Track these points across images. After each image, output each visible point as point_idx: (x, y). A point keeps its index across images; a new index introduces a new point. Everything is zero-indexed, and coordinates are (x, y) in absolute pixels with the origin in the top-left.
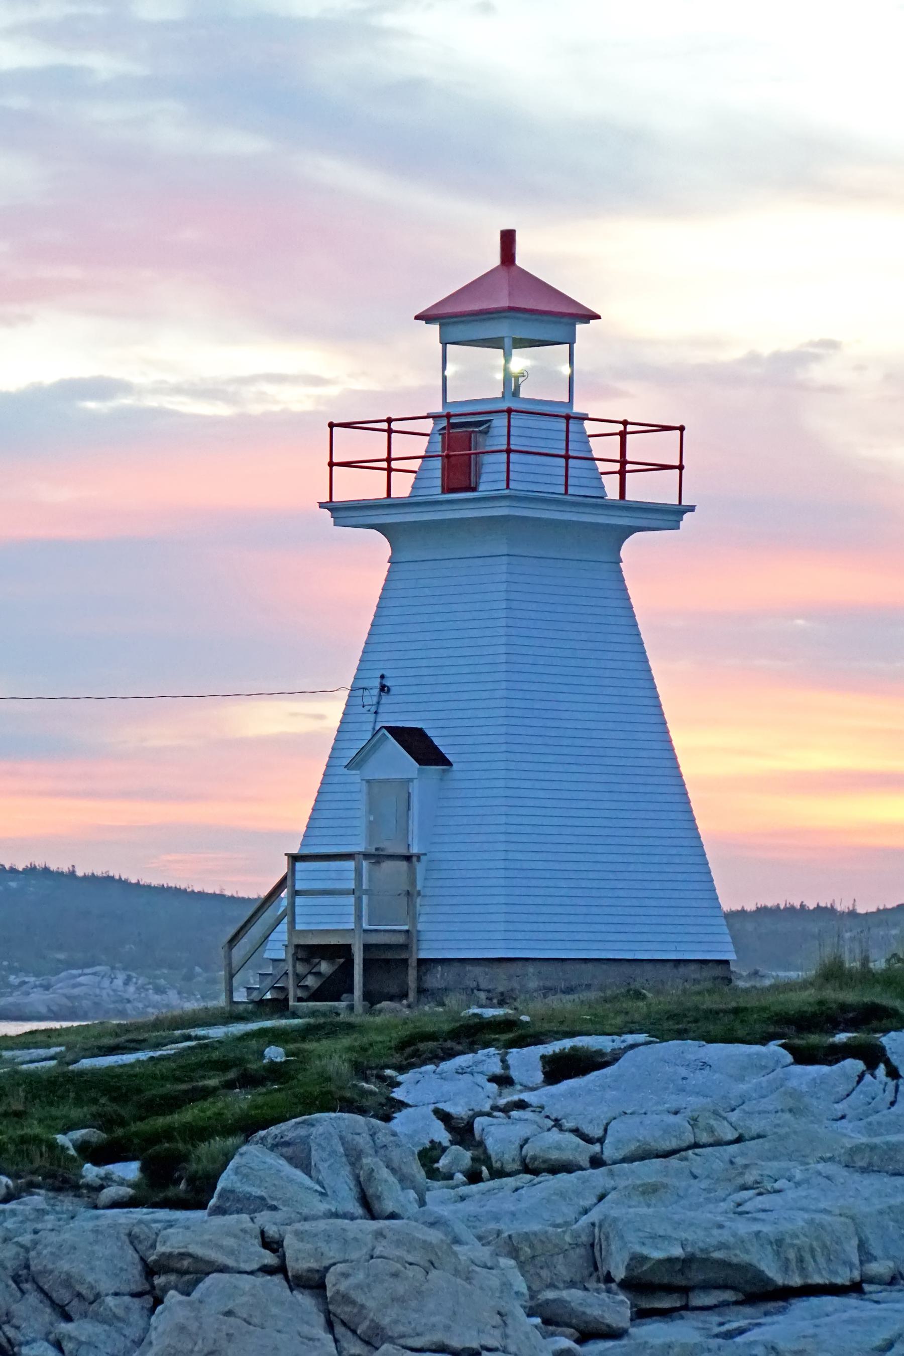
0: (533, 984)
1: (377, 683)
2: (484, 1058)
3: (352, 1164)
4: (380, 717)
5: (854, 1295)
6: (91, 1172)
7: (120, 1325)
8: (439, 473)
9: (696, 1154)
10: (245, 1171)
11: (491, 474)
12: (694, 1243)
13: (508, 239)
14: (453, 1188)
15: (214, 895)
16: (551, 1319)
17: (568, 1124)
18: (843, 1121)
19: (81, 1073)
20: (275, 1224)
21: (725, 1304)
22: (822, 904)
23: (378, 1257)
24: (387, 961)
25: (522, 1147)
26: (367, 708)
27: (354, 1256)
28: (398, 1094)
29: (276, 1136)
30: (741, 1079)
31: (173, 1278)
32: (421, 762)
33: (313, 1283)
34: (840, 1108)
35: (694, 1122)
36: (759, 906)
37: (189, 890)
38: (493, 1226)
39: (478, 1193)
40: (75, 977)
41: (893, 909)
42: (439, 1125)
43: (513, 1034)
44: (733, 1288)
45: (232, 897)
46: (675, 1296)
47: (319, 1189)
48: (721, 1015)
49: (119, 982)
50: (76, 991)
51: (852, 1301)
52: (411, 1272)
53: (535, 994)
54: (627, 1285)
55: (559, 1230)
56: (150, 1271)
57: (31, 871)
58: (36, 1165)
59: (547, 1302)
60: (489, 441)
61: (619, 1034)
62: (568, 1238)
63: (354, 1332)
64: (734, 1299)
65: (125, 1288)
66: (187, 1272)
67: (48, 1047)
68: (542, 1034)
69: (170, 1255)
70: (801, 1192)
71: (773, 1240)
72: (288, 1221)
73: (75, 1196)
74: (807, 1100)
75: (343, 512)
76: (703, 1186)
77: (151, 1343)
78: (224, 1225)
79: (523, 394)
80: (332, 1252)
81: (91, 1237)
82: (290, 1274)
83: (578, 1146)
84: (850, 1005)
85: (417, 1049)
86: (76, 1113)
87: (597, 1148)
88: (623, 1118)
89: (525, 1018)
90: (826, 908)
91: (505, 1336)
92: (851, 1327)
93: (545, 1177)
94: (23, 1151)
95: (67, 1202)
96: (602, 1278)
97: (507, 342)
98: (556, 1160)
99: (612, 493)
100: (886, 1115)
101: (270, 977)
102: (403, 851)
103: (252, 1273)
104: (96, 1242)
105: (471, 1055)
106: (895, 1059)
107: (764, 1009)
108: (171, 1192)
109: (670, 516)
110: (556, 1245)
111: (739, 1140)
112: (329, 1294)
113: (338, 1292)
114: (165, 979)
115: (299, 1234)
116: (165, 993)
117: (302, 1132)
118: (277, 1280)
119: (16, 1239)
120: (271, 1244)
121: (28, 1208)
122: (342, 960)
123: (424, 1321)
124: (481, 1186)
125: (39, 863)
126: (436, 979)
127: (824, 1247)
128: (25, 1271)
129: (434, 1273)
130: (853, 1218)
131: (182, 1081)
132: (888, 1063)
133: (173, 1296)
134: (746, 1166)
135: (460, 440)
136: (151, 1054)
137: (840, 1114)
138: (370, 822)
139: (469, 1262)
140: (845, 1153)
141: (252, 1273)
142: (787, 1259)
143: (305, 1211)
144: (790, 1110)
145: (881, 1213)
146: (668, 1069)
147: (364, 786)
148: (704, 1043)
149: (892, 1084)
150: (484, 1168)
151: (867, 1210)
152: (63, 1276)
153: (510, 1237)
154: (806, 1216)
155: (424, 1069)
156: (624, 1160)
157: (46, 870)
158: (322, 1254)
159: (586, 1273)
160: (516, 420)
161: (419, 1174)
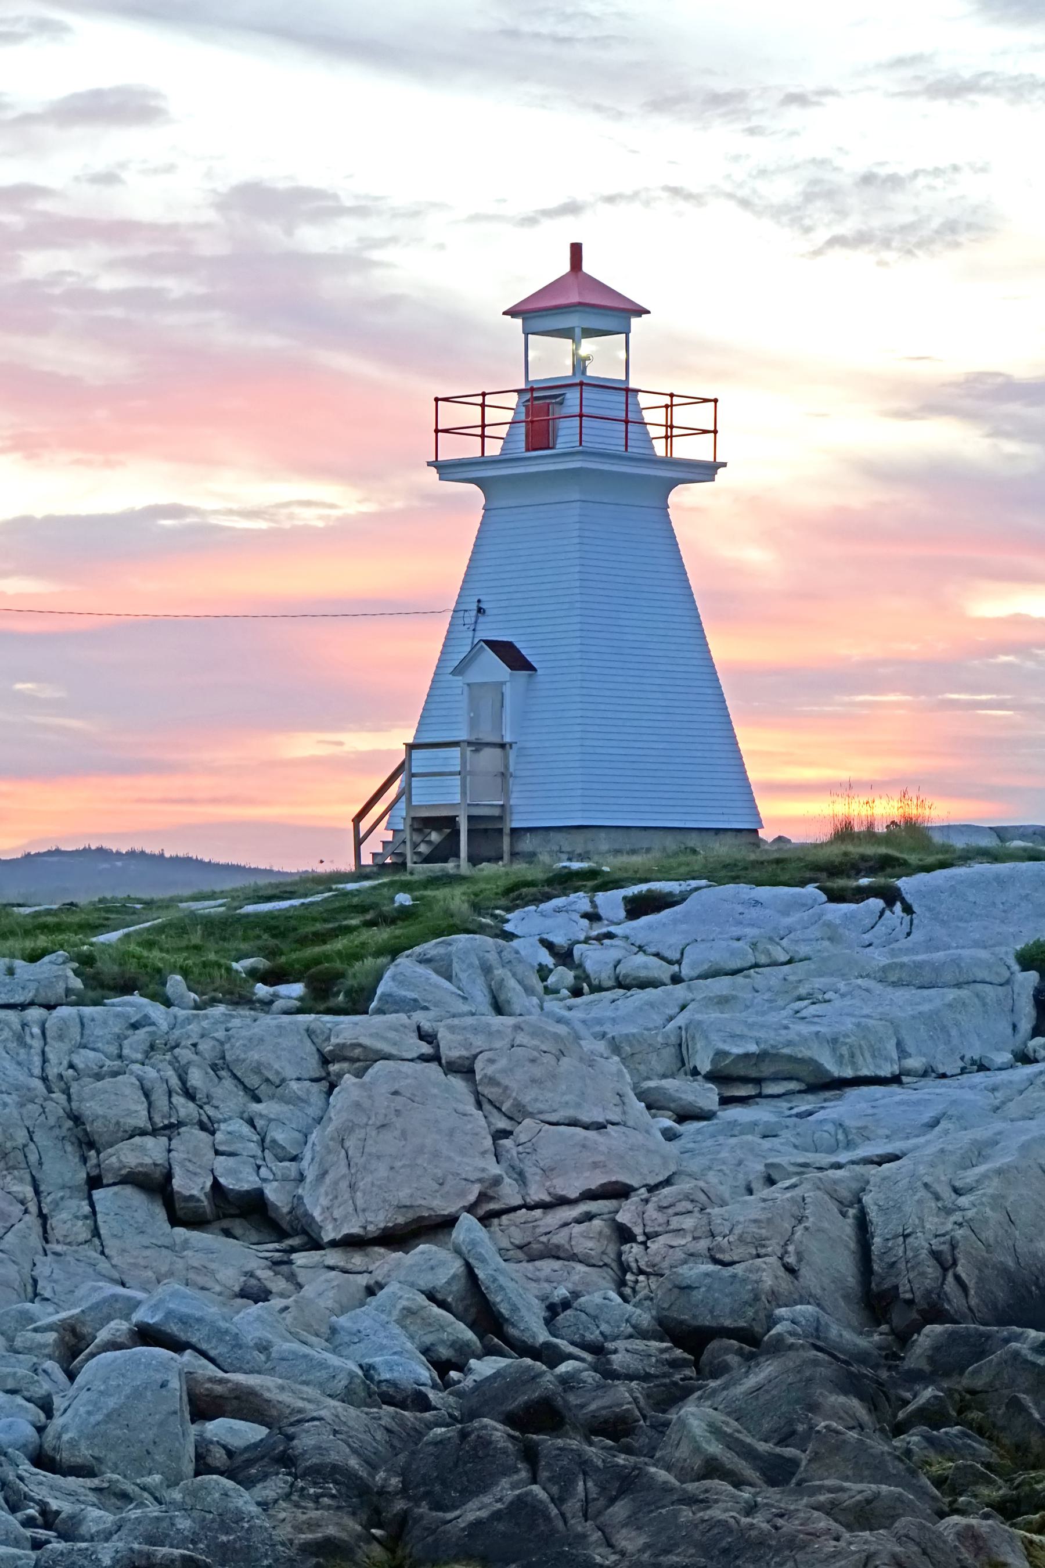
0: (604, 847)
1: (474, 606)
6: (262, 990)
8: (523, 437)
11: (566, 435)
12: (766, 1042)
13: (576, 250)
14: (561, 1000)
15: (265, 870)
17: (653, 950)
19: (247, 915)
24: (486, 830)
25: (615, 967)
27: (498, 1044)
31: (345, 1065)
32: (512, 667)
35: (754, 946)
44: (798, 1079)
51: (894, 1088)
52: (548, 1059)
54: (710, 1077)
56: (325, 1060)
57: (132, 854)
61: (685, 880)
62: (660, 1039)
63: (499, 1109)
66: (358, 1060)
68: (622, 880)
69: (343, 1046)
70: (847, 1001)
75: (446, 469)
77: (330, 1119)
79: (588, 373)
80: (479, 1042)
85: (518, 894)
86: (244, 946)
87: (676, 968)
89: (606, 869)
91: (624, 1113)
92: (903, 1108)
95: (245, 1012)
100: (904, 943)
102: (497, 740)
103: (412, 1060)
104: (280, 1035)
106: (909, 898)
107: (800, 859)
108: (332, 1003)
109: (707, 471)
111: (790, 962)
112: (478, 1078)
113: (485, 1075)
115: (452, 1029)
118: (434, 1066)
120: (424, 1036)
125: (138, 848)
126: (527, 844)
129: (565, 1061)
132: (903, 902)
133: (348, 1079)
135: (541, 411)
136: (302, 900)
141: (412, 1060)
142: (842, 1056)
143: (453, 1010)
144: (829, 939)
145: (913, 1017)
147: (466, 687)
153: (613, 1038)
154: (853, 1020)
156: (699, 977)
157: (143, 853)
159: (675, 1069)
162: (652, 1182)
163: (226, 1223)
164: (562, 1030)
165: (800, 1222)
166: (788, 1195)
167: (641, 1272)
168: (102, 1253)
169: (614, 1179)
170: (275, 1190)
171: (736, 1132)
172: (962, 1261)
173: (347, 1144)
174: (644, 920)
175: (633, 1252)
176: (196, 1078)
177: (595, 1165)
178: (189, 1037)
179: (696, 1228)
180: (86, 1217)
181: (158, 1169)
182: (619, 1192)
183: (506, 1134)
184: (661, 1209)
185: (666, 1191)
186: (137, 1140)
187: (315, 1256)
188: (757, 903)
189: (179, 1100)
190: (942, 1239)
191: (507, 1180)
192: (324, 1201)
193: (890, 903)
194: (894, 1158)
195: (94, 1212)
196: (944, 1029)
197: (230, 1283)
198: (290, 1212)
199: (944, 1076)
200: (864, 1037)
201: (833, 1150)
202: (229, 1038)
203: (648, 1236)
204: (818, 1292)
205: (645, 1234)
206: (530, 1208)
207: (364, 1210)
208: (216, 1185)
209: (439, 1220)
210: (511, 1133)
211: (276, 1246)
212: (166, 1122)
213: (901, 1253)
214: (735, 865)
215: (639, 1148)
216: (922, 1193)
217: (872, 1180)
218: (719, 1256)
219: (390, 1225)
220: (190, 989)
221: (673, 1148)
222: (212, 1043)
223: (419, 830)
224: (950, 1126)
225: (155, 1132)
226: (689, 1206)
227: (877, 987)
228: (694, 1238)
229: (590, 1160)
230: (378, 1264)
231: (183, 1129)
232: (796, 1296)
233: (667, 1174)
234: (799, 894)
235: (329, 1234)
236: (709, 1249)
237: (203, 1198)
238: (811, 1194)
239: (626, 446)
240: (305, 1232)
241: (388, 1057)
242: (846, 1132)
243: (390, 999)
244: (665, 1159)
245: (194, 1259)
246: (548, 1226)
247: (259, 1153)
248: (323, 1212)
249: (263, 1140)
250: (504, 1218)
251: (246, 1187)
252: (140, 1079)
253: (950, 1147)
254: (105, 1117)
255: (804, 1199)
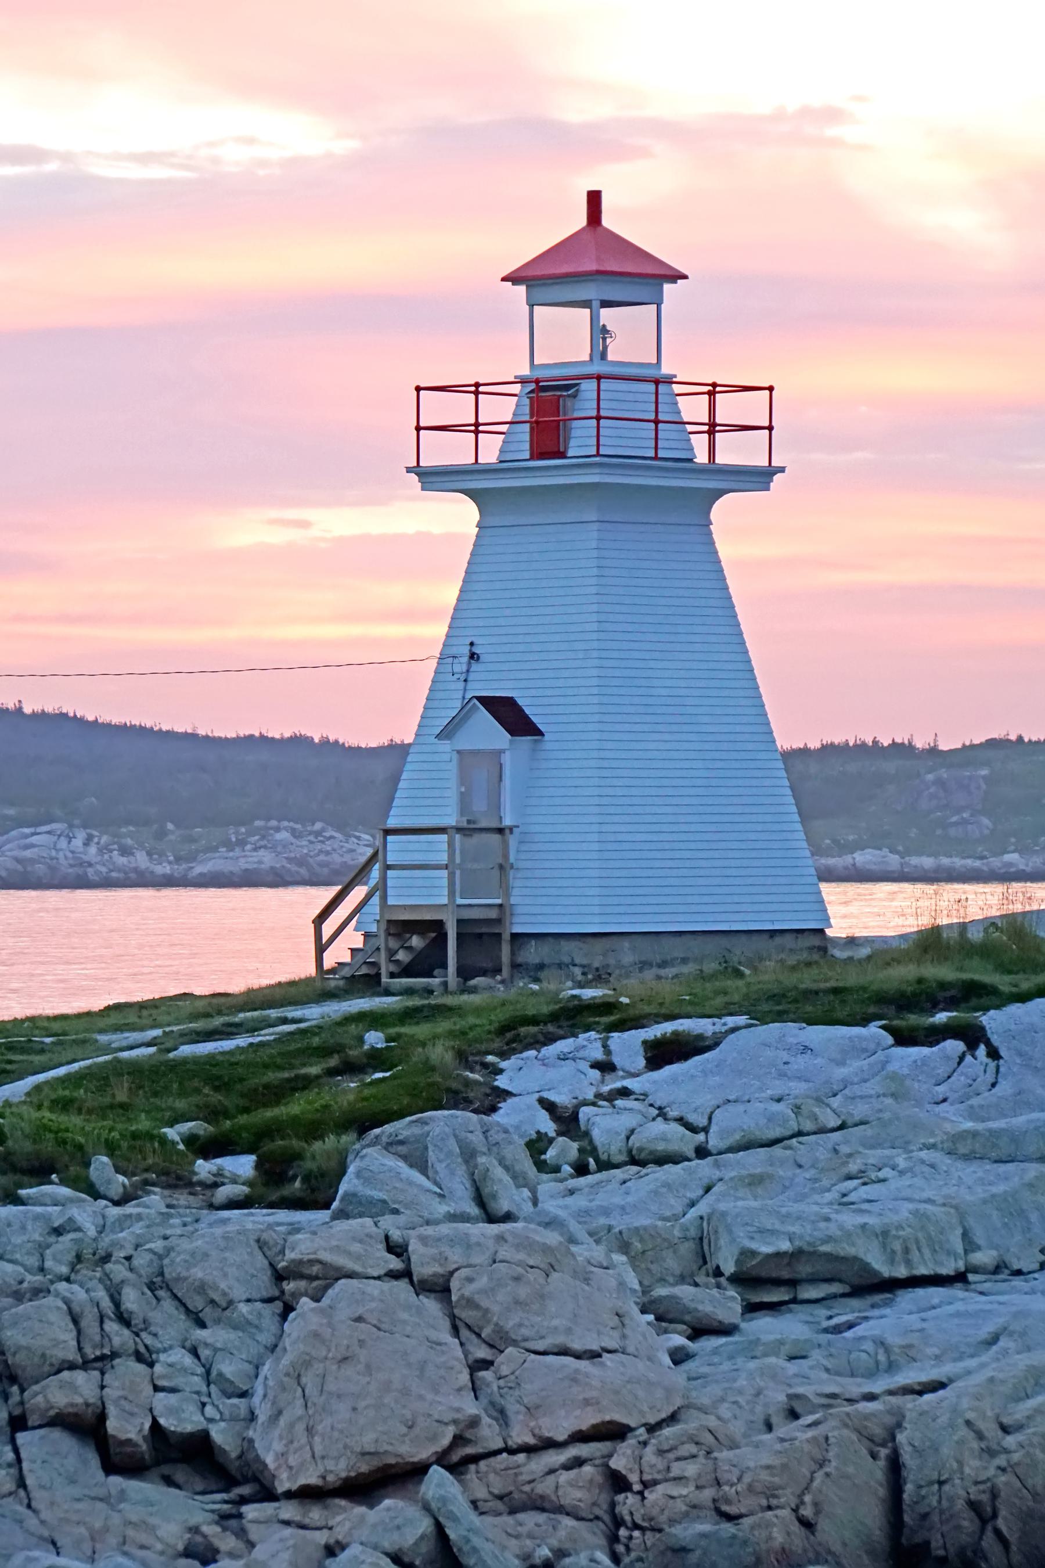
0: (628, 958)
1: (466, 650)
2: (585, 1043)
3: (466, 1162)
4: (470, 685)
5: (959, 1285)
6: (204, 1168)
7: (254, 1330)
8: (527, 437)
9: (800, 1143)
10: (367, 1174)
11: (580, 440)
12: (801, 1237)
13: (594, 199)
14: (561, 1181)
15: (186, 735)
16: (664, 1316)
17: (673, 1113)
18: (945, 1104)
19: (184, 1061)
20: (399, 1228)
21: (835, 1296)
22: (898, 740)
23: (500, 1261)
24: (480, 936)
26: (456, 676)
27: (476, 1260)
28: (501, 1082)
29: (391, 1135)
30: (841, 1063)
31: (302, 1284)
32: (512, 733)
33: (438, 1288)
34: (941, 1090)
35: (797, 1109)
36: (825, 743)
37: (155, 729)
38: (602, 1221)
39: (586, 1186)
40: (27, 836)
41: (981, 744)
42: (544, 1115)
43: (612, 1017)
44: (840, 1281)
45: (207, 736)
46: (783, 1289)
47: (438, 1191)
48: (821, 994)
49: (78, 843)
50: (28, 853)
51: (956, 1292)
52: (532, 1275)
53: (631, 969)
54: (740, 1280)
55: (669, 1224)
56: (279, 1277)
58: (150, 1161)
59: (660, 1299)
60: (578, 404)
61: (719, 1017)
62: (677, 1233)
63: (479, 1335)
64: (841, 1291)
65: (256, 1295)
66: (316, 1278)
67: (142, 1029)
68: (647, 1016)
69: (301, 1262)
70: (906, 1181)
71: (879, 1232)
72: (410, 1225)
73: (191, 1194)
74: (908, 1082)
75: (433, 478)
76: (808, 1177)
77: (285, 1350)
78: (350, 1230)
80: (455, 1257)
81: (222, 1244)
82: (415, 1279)
83: (684, 1135)
84: (950, 983)
85: (519, 1033)
86: (181, 1104)
87: (701, 1137)
88: (726, 1106)
89: (625, 1000)
90: (903, 744)
91: (624, 1337)
93: (651, 1168)
94: (135, 1148)
96: (711, 1271)
97: (596, 304)
98: (663, 1151)
99: (701, 457)
100: (987, 1097)
101: (361, 953)
102: (494, 825)
103: (379, 1278)
105: (571, 1040)
106: (995, 1040)
107: (864, 989)
108: (286, 1191)
109: (760, 477)
110: (665, 1240)
111: (842, 1127)
112: (454, 1298)
113: (462, 1297)
114: (132, 839)
115: (424, 1240)
116: (132, 854)
117: (416, 1130)
118: (403, 1284)
119: (147, 1246)
120: (396, 1249)
121: (153, 1211)
122: (433, 935)
123: (545, 1324)
124: (589, 1179)
126: (531, 954)
127: (929, 1238)
128: (159, 1279)
129: (555, 1275)
130: (956, 1208)
131: (280, 1068)
132: (988, 1044)
133: (305, 1303)
134: (850, 1155)
135: (549, 407)
137: (941, 1097)
138: (462, 793)
139: (586, 1264)
140: (947, 1140)
141: (379, 1278)
142: (893, 1252)
144: (893, 1095)
145: (985, 1202)
146: (769, 1053)
148: (804, 1025)
149: (992, 1065)
150: (591, 1160)
151: (972, 1198)
152: (196, 1283)
153: (620, 1232)
154: (911, 1206)
155: (525, 1054)
158: (446, 1259)
160: (605, 384)
161: (527, 1165)
162: (652, 1420)
163: (166, 1469)
164: (552, 1238)
165: (821, 1466)
166: (810, 1434)
167: (636, 1526)
168: (29, 1506)
169: (607, 1418)
170: (223, 1431)
171: (758, 1354)
172: (1003, 1512)
173: (304, 1380)
174: (668, 1070)
175: (627, 1503)
176: (132, 1299)
177: (587, 1402)
178: (122, 1247)
179: (699, 1475)
180: (10, 1465)
181: (90, 1410)
182: (613, 1433)
183: (486, 1364)
184: (661, 1452)
185: (667, 1431)
186: (66, 1374)
187: (268, 1509)
188: (806, 1049)
189: (112, 1327)
190: (982, 1487)
191: (486, 1420)
192: (278, 1446)
193: (972, 1046)
194: (938, 1386)
195: (19, 1460)
196: (1022, 1213)
197: (172, 1541)
198: (240, 1457)
199: (1019, 1273)
200: (923, 1228)
201: (871, 1374)
202: (169, 1250)
203: (646, 1485)
204: (837, 1548)
205: (642, 1482)
206: (512, 1452)
207: (323, 1458)
208: (155, 1425)
209: (409, 1467)
210: (491, 1363)
211: (224, 1496)
212: (98, 1353)
213: (935, 1503)
214: (784, 996)
215: (639, 1374)
216: (964, 1432)
217: (908, 1414)
218: (725, 1508)
219: (353, 1474)
220: (118, 1170)
221: (678, 1376)
222: (149, 1256)
223: (397, 936)
224: (1011, 1345)
225: (86, 1365)
226: (693, 1449)
227: (944, 1161)
228: (698, 1487)
229: (581, 1397)
230: (339, 1518)
231: (117, 1361)
232: (811, 1555)
233: (671, 1410)
234: (860, 1037)
235: (283, 1484)
236: (714, 1501)
237: (141, 1441)
238: (836, 1433)
239: (656, 448)
240: (255, 1479)
241: (351, 1275)
242: (887, 1350)
243: (354, 1200)
244: (669, 1391)
245: (133, 1513)
246: (533, 1472)
247: (204, 1389)
248: (277, 1459)
249: (208, 1372)
250: (483, 1464)
251: (189, 1428)
252: (67, 1302)
253: (1001, 1376)
254: (28, 1348)
255: (827, 1438)
